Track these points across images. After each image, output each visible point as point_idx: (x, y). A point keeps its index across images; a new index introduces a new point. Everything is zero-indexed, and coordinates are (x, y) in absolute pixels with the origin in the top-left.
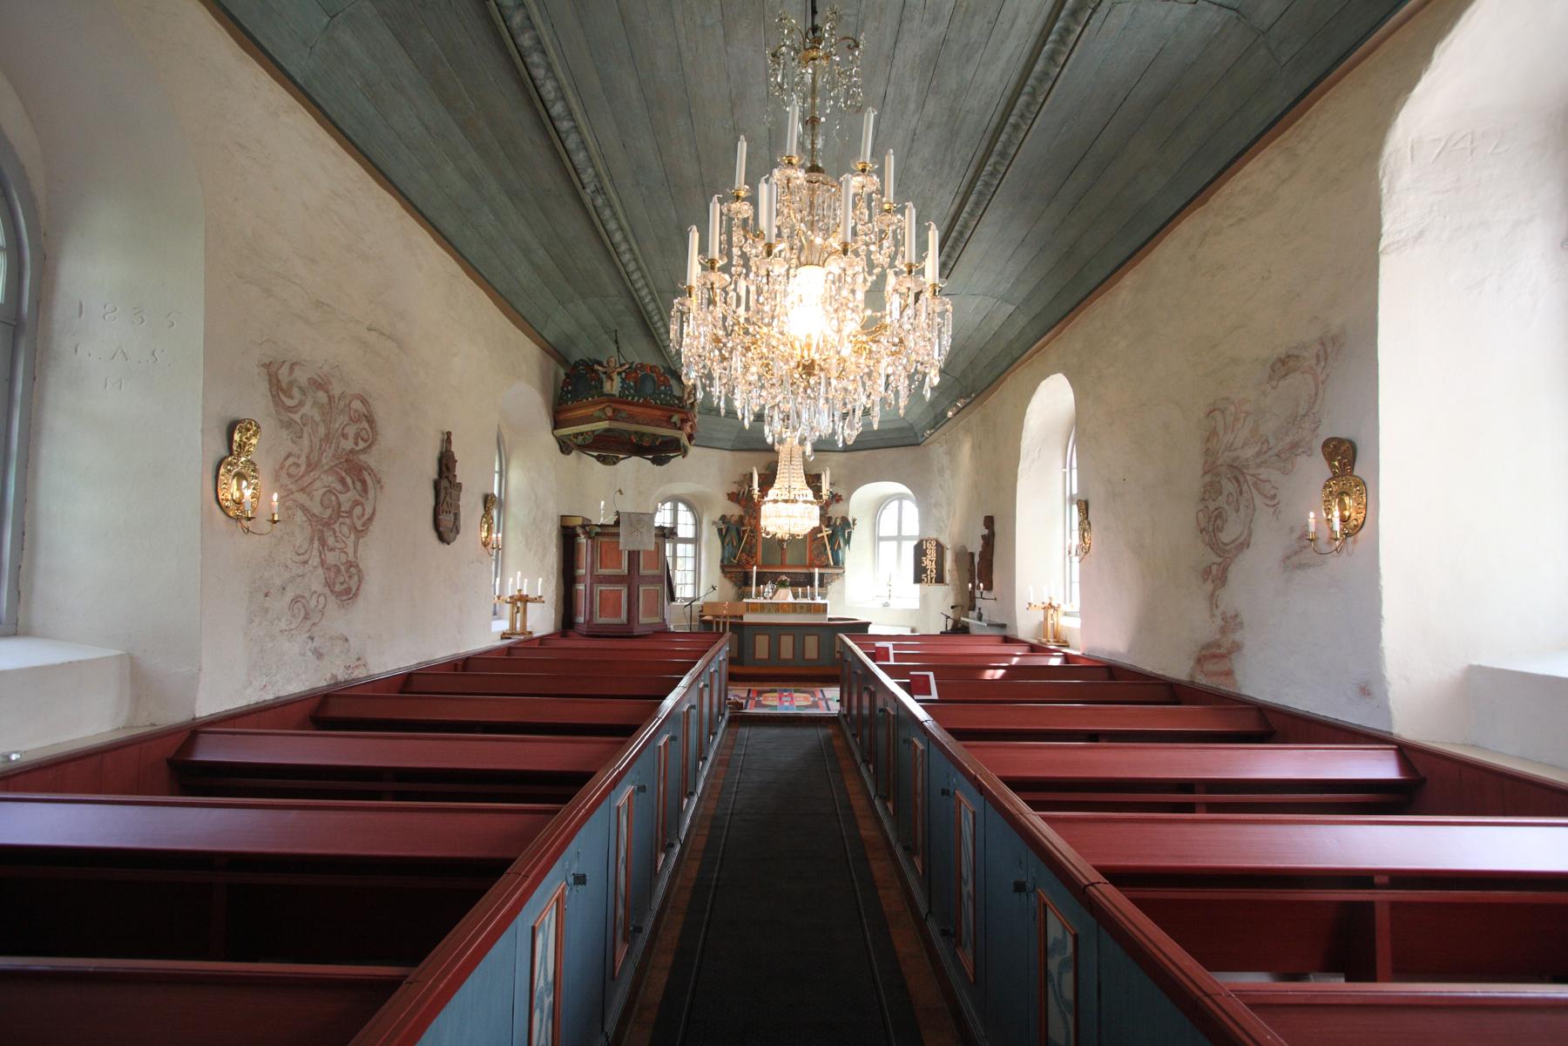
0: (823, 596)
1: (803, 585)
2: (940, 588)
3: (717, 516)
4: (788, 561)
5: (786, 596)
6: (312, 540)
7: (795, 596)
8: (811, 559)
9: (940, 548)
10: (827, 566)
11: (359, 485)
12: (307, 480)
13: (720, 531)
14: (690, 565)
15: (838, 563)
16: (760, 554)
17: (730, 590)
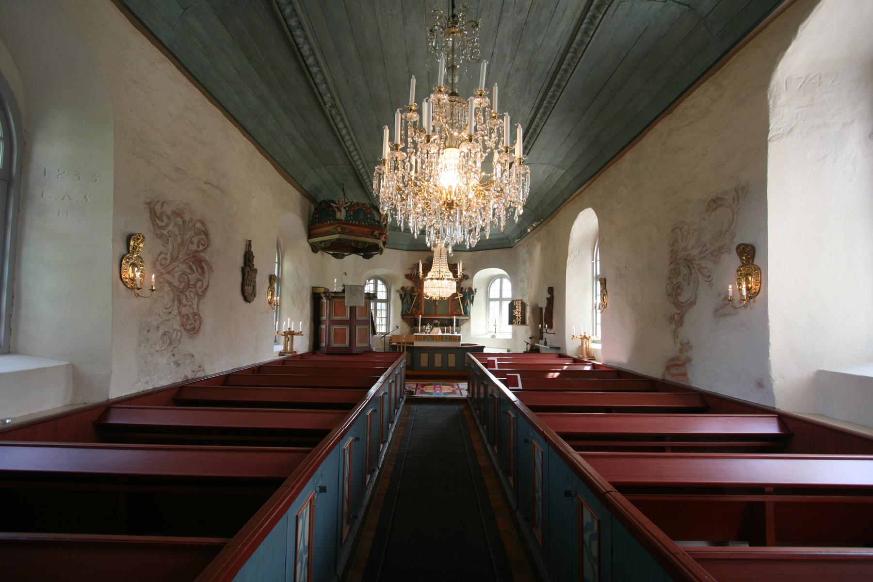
0: (458, 332)
1: (447, 326)
2: (523, 327)
3: (399, 287)
4: (439, 312)
5: (438, 332)
6: (174, 301)
7: (443, 332)
8: (452, 312)
9: (523, 305)
10: (461, 315)
11: (200, 270)
12: (171, 267)
13: (401, 295)
14: (384, 314)
15: (467, 313)
16: (423, 308)
17: (406, 328)
